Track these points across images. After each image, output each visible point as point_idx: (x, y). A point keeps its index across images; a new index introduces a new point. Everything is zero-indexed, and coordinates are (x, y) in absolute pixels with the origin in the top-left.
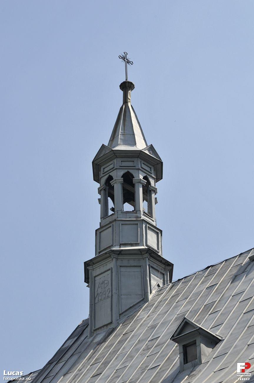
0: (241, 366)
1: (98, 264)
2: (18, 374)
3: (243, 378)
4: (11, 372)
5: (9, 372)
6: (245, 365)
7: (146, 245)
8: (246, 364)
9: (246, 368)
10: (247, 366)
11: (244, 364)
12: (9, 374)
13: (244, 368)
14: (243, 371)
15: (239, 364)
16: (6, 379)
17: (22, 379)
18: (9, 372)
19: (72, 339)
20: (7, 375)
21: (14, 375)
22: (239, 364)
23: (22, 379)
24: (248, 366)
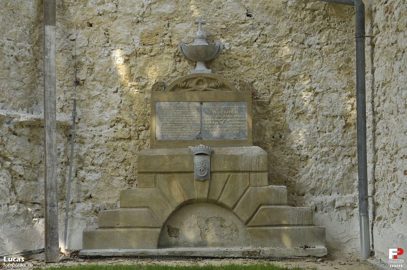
0: (393, 252)
1: (182, 191)
2: (20, 261)
3: (395, 265)
4: (12, 258)
5: (9, 259)
6: (398, 250)
7: (374, 203)
8: (399, 249)
9: (398, 254)
10: (399, 252)
11: (396, 250)
12: (9, 261)
13: (396, 254)
14: (395, 257)
15: (391, 250)
16: (7, 266)
17: (23, 265)
18: (9, 259)
19: (191, 256)
20: (7, 261)
21: (15, 261)
22: (391, 250)
23: (23, 265)
24: (401, 251)
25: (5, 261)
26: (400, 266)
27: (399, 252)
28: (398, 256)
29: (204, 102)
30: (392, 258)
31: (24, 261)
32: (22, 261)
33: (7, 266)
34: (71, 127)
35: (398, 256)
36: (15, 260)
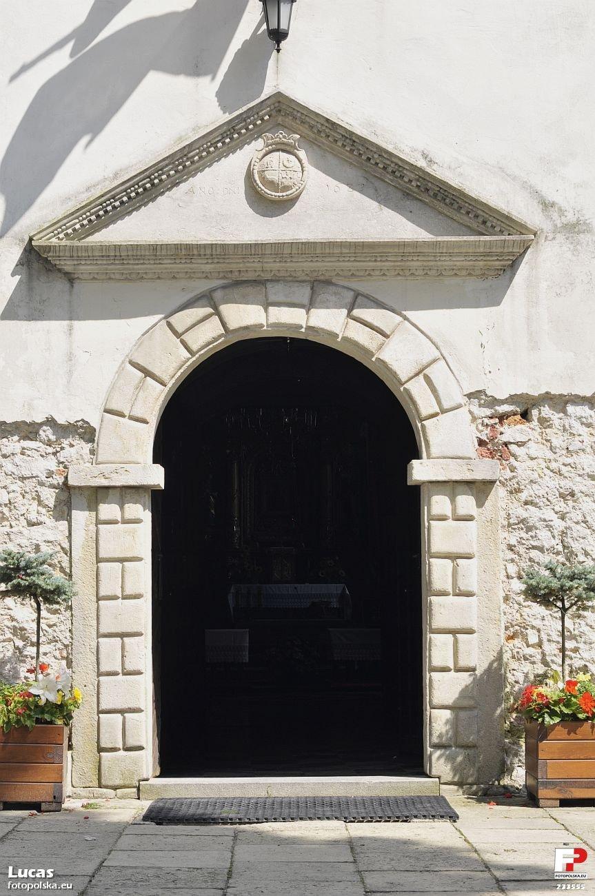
2: (43, 876)
4: (26, 871)
5: (20, 871)
6: (575, 853)
10: (577, 856)
12: (20, 875)
13: (571, 861)
16: (14, 886)
18: (20, 871)
20: (16, 876)
21: (34, 876)
25: (10, 875)
26: (579, 888)
27: (577, 856)
28: (576, 866)
29: (98, 742)
30: (561, 870)
31: (54, 877)
32: (48, 876)
33: (14, 886)
34: (61, 711)
35: (576, 866)
36: (33, 873)
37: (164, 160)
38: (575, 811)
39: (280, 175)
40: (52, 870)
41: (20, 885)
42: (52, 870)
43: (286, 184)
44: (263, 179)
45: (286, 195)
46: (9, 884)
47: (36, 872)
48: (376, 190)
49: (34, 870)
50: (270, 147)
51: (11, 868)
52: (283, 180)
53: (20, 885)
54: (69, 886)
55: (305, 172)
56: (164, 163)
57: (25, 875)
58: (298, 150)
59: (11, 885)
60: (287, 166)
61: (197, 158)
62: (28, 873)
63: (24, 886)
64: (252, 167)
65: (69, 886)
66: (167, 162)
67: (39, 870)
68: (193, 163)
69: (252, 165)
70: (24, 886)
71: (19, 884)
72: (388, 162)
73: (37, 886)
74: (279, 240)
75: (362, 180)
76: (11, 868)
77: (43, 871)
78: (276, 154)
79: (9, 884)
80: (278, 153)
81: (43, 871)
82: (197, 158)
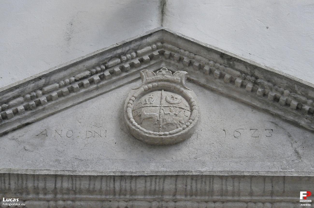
2: (15, 201)
4: (9, 199)
5: (7, 199)
12: (7, 201)
18: (7, 199)
20: (5, 201)
21: (12, 201)
32: (17, 201)
36: (12, 200)
37: (11, 90)
38: (131, 38)
39: (162, 111)
40: (18, 199)
41: (7, 204)
42: (18, 199)
43: (169, 120)
44: (139, 117)
45: (170, 134)
46: (3, 204)
47: (13, 200)
48: (290, 136)
49: (12, 199)
50: (150, 85)
51: (4, 198)
52: (166, 117)
53: (7, 204)
54: (24, 204)
55: (194, 111)
56: (10, 94)
57: (9, 201)
58: (185, 88)
59: (4, 204)
60: (172, 102)
61: (54, 94)
62: (10, 200)
63: (8, 205)
64: (125, 106)
65: (24, 204)
66: (16, 92)
67: (14, 199)
68: (50, 99)
69: (126, 103)
70: (8, 205)
71: (7, 204)
72: (304, 99)
73: (13, 205)
74: (157, 172)
75: (269, 126)
76: (4, 198)
77: (15, 199)
78: (157, 94)
79: (3, 204)
80: (160, 92)
81: (15, 199)
82: (54, 94)
